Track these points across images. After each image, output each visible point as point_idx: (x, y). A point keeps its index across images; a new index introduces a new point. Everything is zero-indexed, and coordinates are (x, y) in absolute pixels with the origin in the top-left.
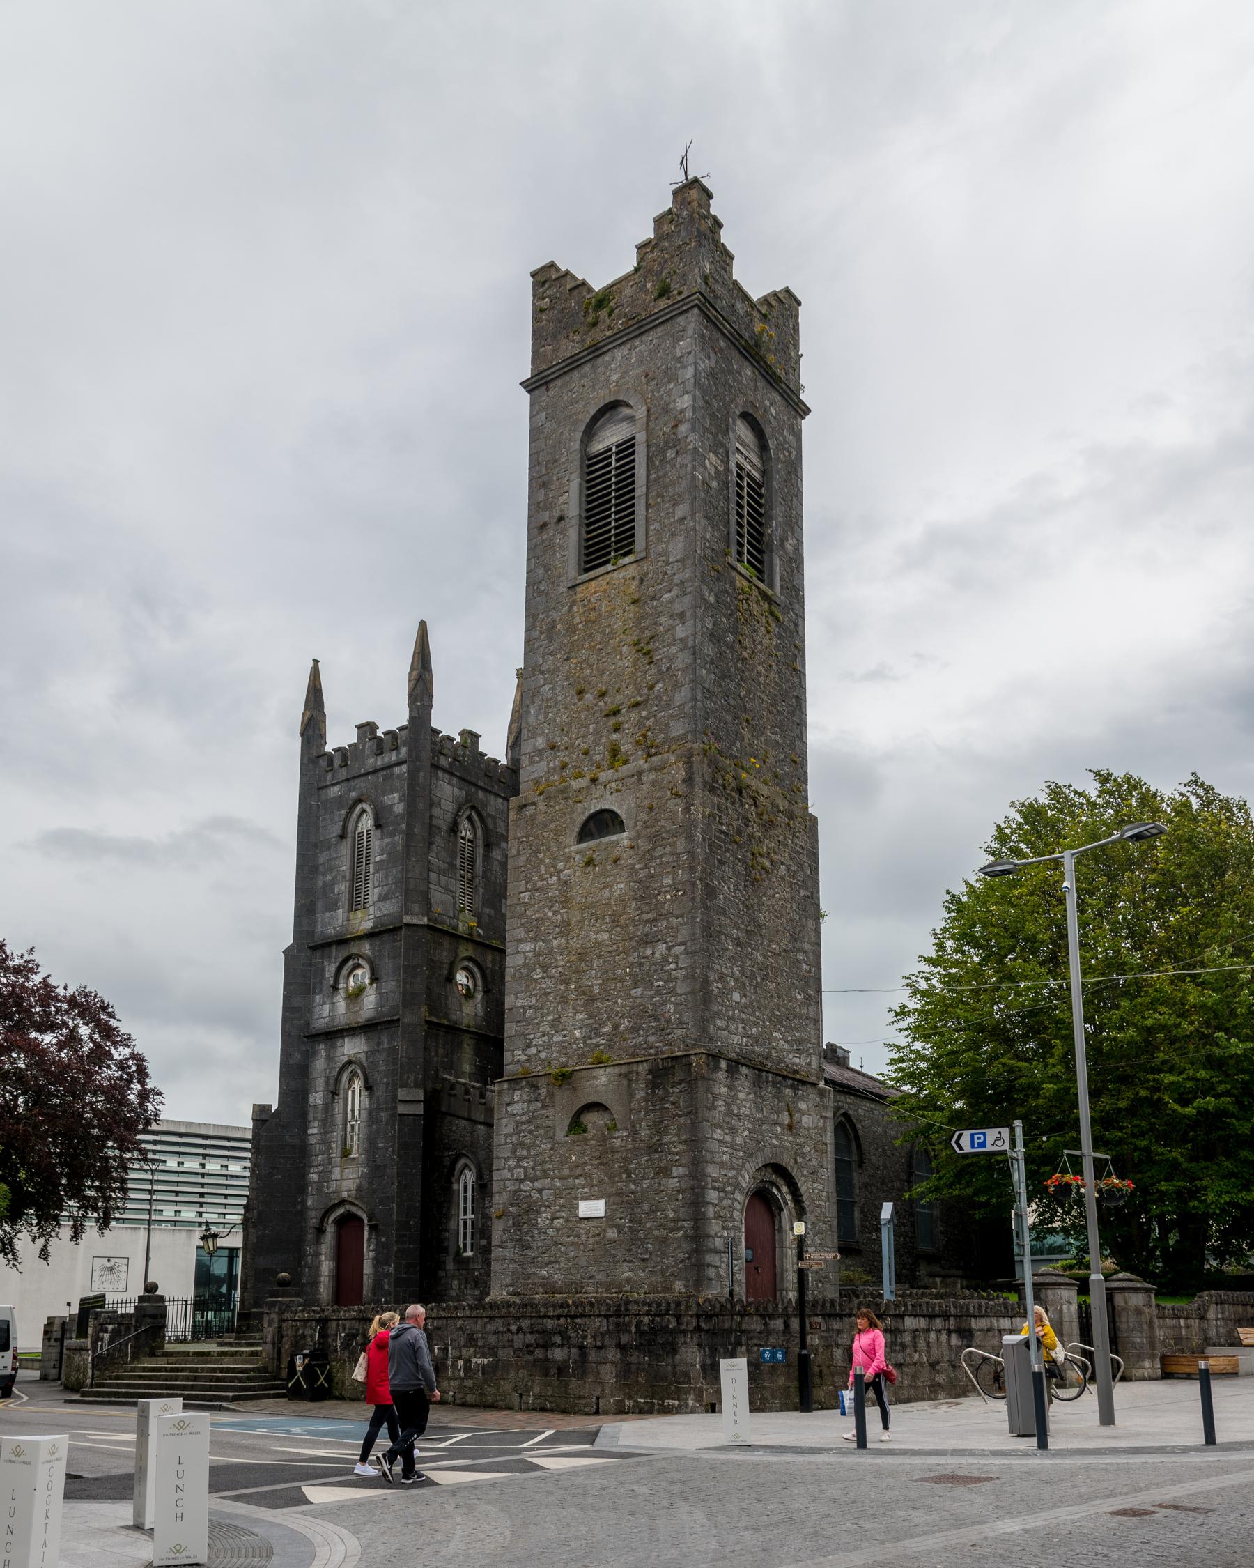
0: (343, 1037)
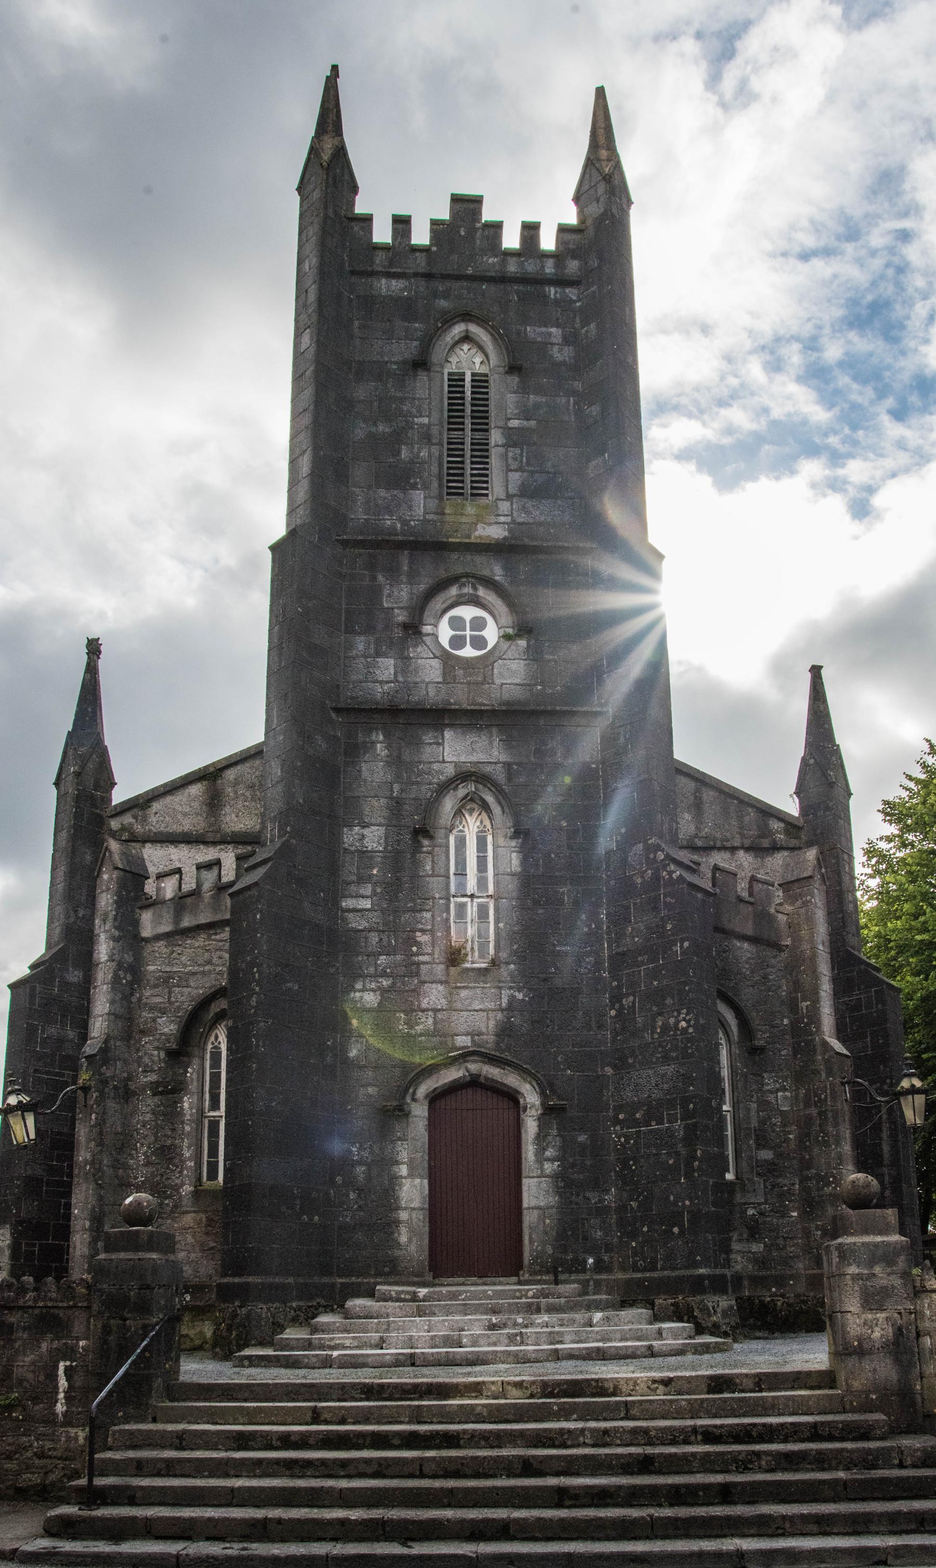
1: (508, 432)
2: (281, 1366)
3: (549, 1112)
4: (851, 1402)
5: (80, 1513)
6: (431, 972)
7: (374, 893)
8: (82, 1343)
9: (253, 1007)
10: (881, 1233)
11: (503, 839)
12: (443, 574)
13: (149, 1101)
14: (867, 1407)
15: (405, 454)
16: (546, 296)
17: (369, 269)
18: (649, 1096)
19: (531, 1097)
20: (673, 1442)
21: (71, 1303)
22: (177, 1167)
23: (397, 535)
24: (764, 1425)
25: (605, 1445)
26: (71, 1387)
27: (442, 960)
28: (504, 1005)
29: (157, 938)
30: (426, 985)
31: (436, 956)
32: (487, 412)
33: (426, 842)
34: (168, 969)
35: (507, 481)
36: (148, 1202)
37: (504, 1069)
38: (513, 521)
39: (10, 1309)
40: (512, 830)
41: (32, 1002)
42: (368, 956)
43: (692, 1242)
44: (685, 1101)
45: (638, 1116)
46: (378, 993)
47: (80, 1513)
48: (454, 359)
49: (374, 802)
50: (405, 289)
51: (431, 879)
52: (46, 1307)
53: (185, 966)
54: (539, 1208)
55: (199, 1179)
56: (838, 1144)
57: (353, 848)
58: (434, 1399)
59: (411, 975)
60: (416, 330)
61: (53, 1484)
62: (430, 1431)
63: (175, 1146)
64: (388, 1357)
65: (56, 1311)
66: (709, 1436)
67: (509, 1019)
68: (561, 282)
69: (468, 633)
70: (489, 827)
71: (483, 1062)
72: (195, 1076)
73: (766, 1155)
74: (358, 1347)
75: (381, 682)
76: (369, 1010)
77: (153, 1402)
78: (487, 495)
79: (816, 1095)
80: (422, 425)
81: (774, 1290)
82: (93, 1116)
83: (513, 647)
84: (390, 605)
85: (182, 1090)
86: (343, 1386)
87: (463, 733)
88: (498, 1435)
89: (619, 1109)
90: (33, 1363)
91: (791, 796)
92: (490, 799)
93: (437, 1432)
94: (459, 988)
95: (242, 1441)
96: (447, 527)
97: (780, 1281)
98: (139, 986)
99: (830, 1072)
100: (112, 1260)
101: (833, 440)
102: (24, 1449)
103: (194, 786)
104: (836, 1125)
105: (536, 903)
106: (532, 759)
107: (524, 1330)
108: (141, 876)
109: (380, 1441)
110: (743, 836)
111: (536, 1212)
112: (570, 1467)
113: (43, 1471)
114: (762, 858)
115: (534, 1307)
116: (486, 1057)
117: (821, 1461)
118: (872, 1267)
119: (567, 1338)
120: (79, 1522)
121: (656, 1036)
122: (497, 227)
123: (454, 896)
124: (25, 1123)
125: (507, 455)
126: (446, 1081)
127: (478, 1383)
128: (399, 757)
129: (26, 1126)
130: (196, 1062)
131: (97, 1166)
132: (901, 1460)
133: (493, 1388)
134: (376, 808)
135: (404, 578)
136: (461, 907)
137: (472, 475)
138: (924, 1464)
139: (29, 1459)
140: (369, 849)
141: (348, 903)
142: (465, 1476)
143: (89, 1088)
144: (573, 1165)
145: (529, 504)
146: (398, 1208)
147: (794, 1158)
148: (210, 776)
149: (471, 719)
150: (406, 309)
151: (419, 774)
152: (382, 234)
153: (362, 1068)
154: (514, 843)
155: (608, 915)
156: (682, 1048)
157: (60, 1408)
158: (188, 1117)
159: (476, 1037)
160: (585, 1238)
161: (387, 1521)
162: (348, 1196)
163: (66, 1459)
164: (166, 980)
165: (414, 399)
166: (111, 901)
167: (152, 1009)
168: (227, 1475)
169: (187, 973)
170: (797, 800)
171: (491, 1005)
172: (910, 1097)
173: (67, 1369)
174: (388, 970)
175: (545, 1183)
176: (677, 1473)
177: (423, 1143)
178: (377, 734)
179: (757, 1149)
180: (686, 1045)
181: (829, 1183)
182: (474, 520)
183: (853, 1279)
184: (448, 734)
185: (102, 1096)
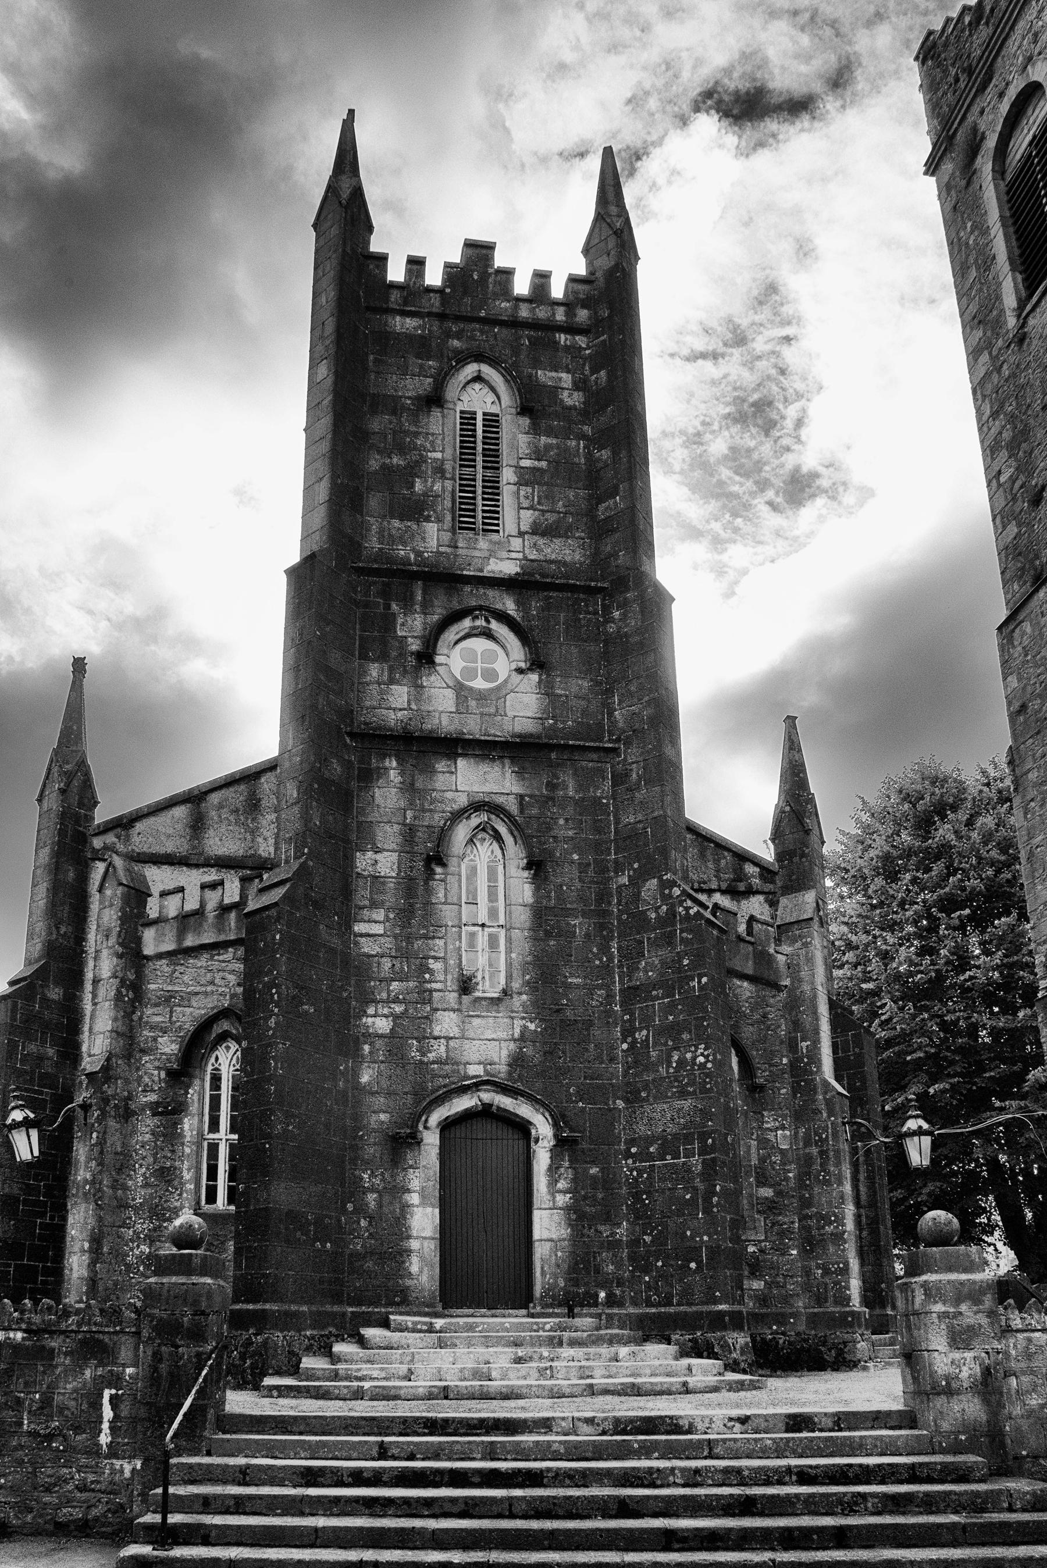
0: (453, 756)
1: (519, 469)
2: (311, 1397)
3: (562, 1145)
4: (940, 1443)
5: (156, 1553)
6: (442, 999)
8: (129, 1371)
9: (271, 1028)
10: (966, 1270)
12: (456, 605)
13: (148, 1122)
14: (957, 1449)
15: (418, 486)
16: (557, 343)
17: (384, 306)
19: (543, 1127)
20: (767, 1483)
21: (118, 1328)
22: (177, 1189)
23: (411, 565)
24: (860, 1465)
25: (696, 1485)
26: (116, 1417)
27: (455, 988)
28: (516, 1036)
29: (160, 956)
31: (449, 984)
32: (498, 450)
33: (439, 870)
34: (170, 988)
35: (519, 518)
36: (199, 1224)
37: (516, 1099)
38: (525, 558)
39: (52, 1333)
40: (525, 861)
41: (13, 1018)
43: (711, 1277)
44: (703, 1137)
45: (651, 1150)
47: (156, 1553)
48: (465, 397)
49: (387, 827)
50: (419, 327)
52: (91, 1332)
53: (187, 985)
55: (198, 1203)
56: (840, 1183)
58: (502, 1435)
60: (430, 367)
61: (96, 1519)
62: (512, 1469)
63: (175, 1168)
64: (421, 1390)
65: (101, 1336)
66: (804, 1477)
67: (521, 1049)
68: (571, 329)
69: (479, 664)
70: (500, 856)
71: (494, 1091)
72: (196, 1098)
73: (767, 1192)
74: (385, 1379)
75: (394, 709)
76: (381, 1036)
77: (206, 1433)
78: (498, 531)
79: (816, 1134)
80: (435, 460)
81: (775, 1327)
82: (94, 1135)
83: (525, 681)
84: (404, 634)
85: (183, 1111)
86: (405, 1420)
87: (477, 763)
88: (584, 1473)
89: (632, 1142)
90: (75, 1390)
91: (765, 841)
92: (503, 830)
93: (519, 1470)
94: (473, 1016)
95: (311, 1477)
96: (460, 560)
97: (781, 1319)
98: (140, 1004)
99: (831, 1113)
100: (163, 1284)
101: (717, 526)
102: (65, 1481)
103: (178, 808)
104: (838, 1164)
105: (548, 934)
107: (554, 1364)
108: (143, 893)
109: (458, 1479)
110: (719, 879)
111: (548, 1245)
112: (669, 1508)
113: (85, 1505)
114: (738, 901)
115: (556, 1341)
116: (497, 1087)
117: (929, 1504)
118: (958, 1305)
119: (597, 1373)
120: (156, 1563)
121: (671, 1070)
122: (507, 273)
124: (29, 1139)
125: (518, 493)
127: (548, 1419)
128: (412, 784)
129: (30, 1143)
130: (197, 1082)
131: (97, 1186)
132: (1010, 1504)
133: (564, 1424)
134: (389, 835)
135: (417, 607)
136: (472, 935)
137: (484, 511)
138: (1034, 1509)
139: (69, 1492)
140: (382, 874)
141: (359, 928)
142: (557, 1517)
143: (90, 1106)
144: (585, 1198)
145: (541, 541)
146: (409, 1237)
147: (793, 1196)
148: (195, 798)
149: (485, 749)
150: (421, 346)
152: (396, 273)
154: (526, 874)
157: (104, 1439)
158: (188, 1139)
160: (597, 1271)
161: (493, 1565)
162: (359, 1223)
163: (110, 1493)
164: (167, 999)
165: (427, 434)
166: (115, 917)
167: (152, 1028)
168: (302, 1514)
169: (189, 993)
170: (771, 846)
172: (916, 1139)
173: (112, 1398)
175: (558, 1216)
176: (781, 1515)
177: (435, 1172)
178: (391, 761)
179: (757, 1186)
181: (831, 1223)
182: (487, 554)
183: (939, 1317)
184: (461, 763)
185: (104, 1115)
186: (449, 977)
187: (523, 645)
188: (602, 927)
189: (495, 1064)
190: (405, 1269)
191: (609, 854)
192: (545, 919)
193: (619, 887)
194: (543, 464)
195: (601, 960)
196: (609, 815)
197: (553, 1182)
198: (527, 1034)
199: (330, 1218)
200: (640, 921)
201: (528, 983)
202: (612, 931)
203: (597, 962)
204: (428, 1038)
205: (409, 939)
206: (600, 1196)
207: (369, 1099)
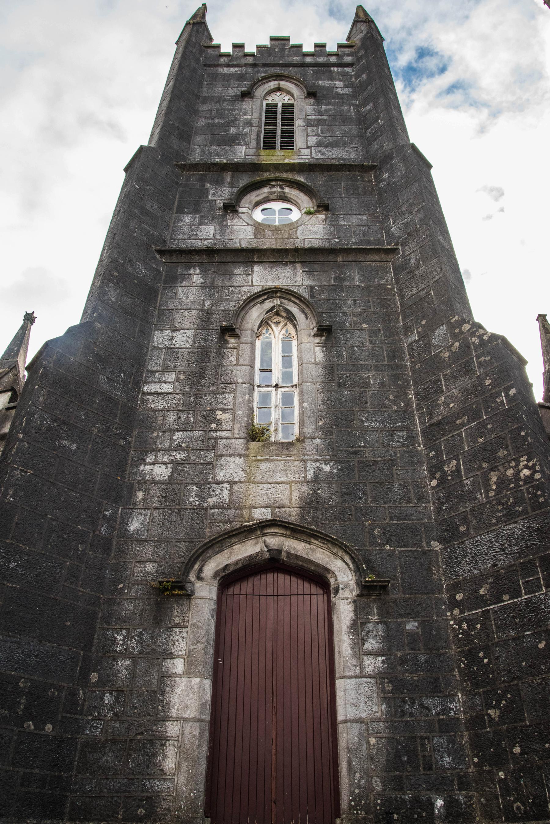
0: (250, 263)
3: (371, 591)
7: (178, 380)
11: (306, 337)
18: (495, 565)
19: (343, 574)
27: (243, 435)
28: (309, 477)
30: (223, 458)
31: (236, 431)
33: (232, 340)
37: (309, 543)
40: (316, 329)
42: (164, 432)
45: (482, 592)
46: (170, 466)
49: (186, 313)
51: (235, 368)
54: (359, 721)
57: (162, 346)
59: (208, 449)
67: (315, 491)
71: (283, 535)
75: (201, 240)
76: (156, 483)
84: (214, 198)
89: (455, 587)
92: (294, 310)
106: (333, 283)
111: (356, 727)
123: (258, 386)
126: (240, 557)
128: (212, 284)
135: (227, 185)
136: (265, 398)
140: (177, 346)
144: (403, 662)
145: (324, 150)
146: (166, 718)
151: (230, 293)
153: (141, 541)
154: (317, 340)
155: (416, 394)
156: (530, 499)
159: (277, 510)
160: (429, 767)
162: (102, 699)
171: (296, 478)
174: (184, 445)
175: (367, 686)
177: (208, 632)
180: (535, 495)
184: (256, 268)
186: (237, 426)
187: (311, 199)
188: (397, 377)
189: (284, 506)
190: (155, 765)
191: (398, 322)
192: (337, 375)
193: (410, 345)
194: (325, 117)
195: (398, 405)
196: (394, 295)
197: (358, 643)
198: (322, 476)
199: (60, 689)
200: (437, 363)
201: (321, 428)
202: (408, 381)
203: (395, 408)
204: (210, 483)
205: (197, 395)
206: (422, 658)
207: (135, 548)
